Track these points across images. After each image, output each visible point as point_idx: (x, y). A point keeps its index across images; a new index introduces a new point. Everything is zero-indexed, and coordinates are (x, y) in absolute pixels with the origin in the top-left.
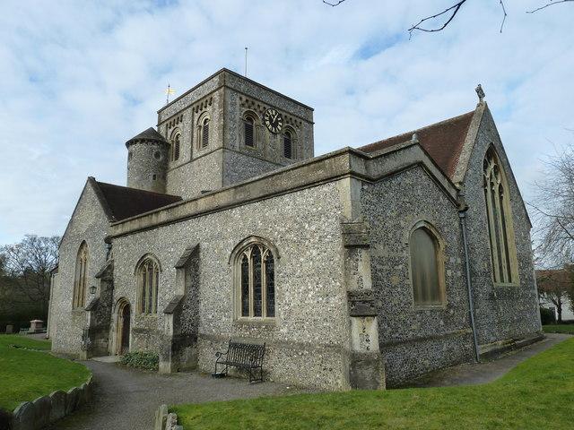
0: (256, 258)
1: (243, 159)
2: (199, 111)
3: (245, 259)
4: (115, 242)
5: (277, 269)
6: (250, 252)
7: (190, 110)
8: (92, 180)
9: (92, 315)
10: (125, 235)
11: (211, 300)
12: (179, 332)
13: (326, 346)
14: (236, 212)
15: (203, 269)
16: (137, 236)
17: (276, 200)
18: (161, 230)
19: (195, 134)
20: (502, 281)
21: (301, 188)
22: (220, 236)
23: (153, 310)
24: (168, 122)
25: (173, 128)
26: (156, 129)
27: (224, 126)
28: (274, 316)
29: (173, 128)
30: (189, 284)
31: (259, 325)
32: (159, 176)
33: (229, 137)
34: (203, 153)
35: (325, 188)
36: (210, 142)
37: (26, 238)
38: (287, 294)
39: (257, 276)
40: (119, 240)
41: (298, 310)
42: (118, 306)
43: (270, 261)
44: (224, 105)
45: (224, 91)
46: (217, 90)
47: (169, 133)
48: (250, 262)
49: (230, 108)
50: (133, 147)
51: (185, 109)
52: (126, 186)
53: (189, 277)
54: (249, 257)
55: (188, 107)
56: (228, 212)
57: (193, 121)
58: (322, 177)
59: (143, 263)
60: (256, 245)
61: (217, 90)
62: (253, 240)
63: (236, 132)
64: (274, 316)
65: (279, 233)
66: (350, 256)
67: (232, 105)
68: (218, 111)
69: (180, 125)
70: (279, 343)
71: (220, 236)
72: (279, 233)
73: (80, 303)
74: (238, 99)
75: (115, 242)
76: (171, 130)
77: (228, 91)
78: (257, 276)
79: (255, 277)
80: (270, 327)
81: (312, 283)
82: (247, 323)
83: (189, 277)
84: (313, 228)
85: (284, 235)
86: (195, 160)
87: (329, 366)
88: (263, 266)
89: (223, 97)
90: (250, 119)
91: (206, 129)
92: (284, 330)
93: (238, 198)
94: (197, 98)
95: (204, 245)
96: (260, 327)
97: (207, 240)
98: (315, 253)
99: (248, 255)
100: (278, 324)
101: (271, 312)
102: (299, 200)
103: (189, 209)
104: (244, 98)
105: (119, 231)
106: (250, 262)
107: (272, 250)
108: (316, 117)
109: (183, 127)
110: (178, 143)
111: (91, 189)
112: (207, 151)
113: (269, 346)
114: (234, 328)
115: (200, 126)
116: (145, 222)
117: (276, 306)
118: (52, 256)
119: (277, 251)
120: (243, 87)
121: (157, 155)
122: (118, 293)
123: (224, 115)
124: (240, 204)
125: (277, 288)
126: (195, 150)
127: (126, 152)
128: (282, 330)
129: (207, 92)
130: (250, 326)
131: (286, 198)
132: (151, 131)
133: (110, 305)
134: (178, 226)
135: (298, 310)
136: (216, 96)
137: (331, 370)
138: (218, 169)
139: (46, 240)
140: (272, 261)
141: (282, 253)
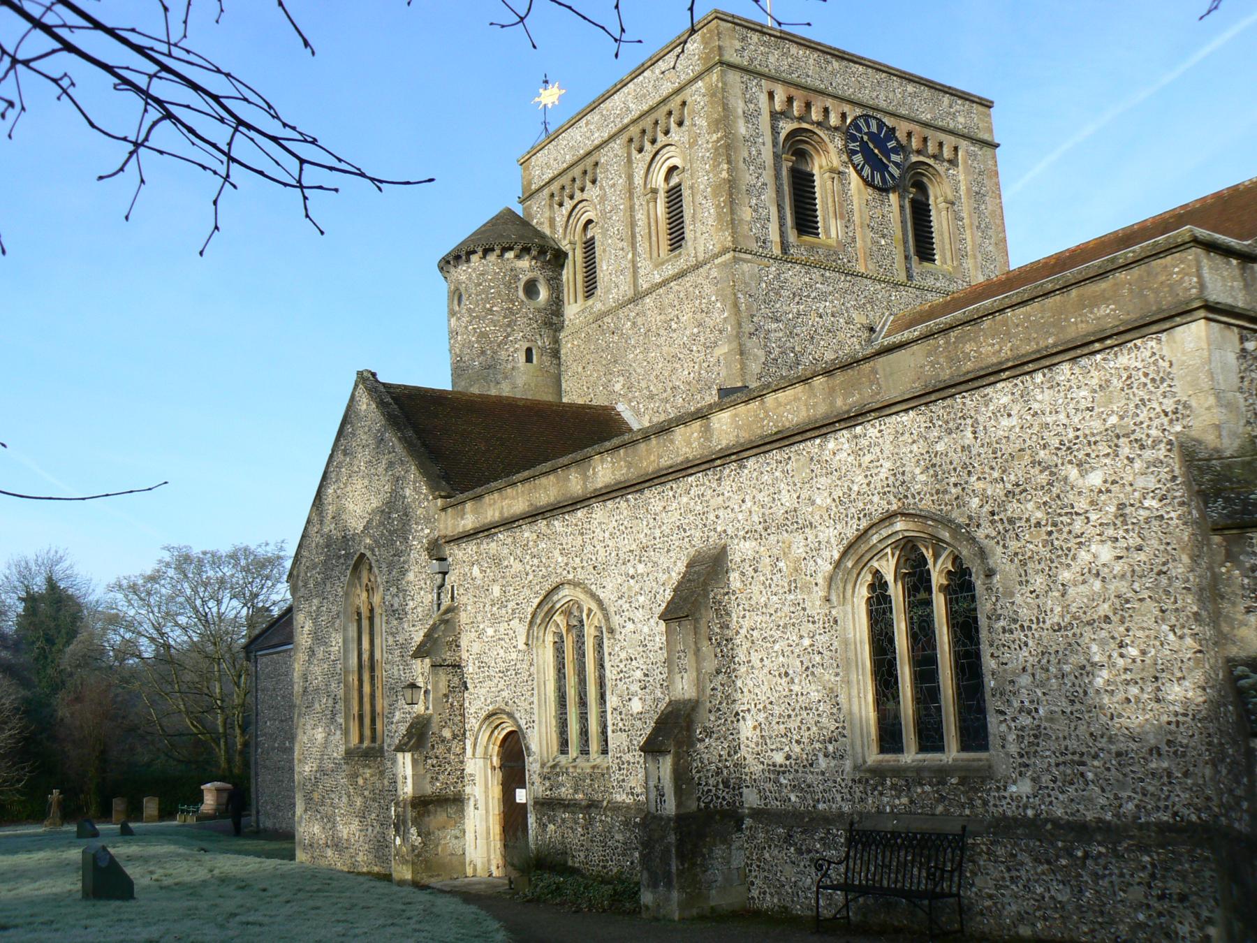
0: (917, 580)
1: (795, 277)
2: (648, 146)
3: (878, 585)
4: (457, 554)
5: (985, 606)
6: (893, 562)
7: (617, 146)
8: (367, 380)
9: (415, 762)
10: (484, 532)
11: (777, 710)
12: (683, 811)
13: (1162, 828)
14: (839, 446)
15: (742, 621)
16: (527, 533)
17: (968, 402)
18: (599, 513)
19: (640, 216)
20: (585, 752)
21: (1044, 360)
22: (794, 522)
23: (594, 746)
24: (555, 187)
25: (568, 204)
26: (519, 210)
27: (732, 185)
28: (985, 747)
29: (568, 204)
30: (710, 665)
31: (942, 773)
32: (542, 350)
33: (746, 214)
34: (670, 270)
35: (1128, 359)
36: (688, 235)
37: (167, 557)
38: (1025, 680)
39: (922, 633)
40: (471, 548)
41: (1061, 726)
42: (483, 737)
43: (960, 584)
44: (723, 121)
45: (723, 75)
46: (698, 77)
47: (560, 220)
48: (896, 592)
49: (742, 129)
50: (462, 273)
51: (605, 143)
52: (450, 389)
53: (706, 648)
54: (889, 578)
55: (612, 138)
56: (813, 447)
57: (630, 177)
58: (1110, 323)
59: (550, 614)
60: (908, 540)
61: (698, 77)
62: (900, 525)
63: (769, 196)
64: (985, 747)
65: (985, 499)
66: (1230, 557)
67: (748, 117)
68: (709, 140)
69: (592, 192)
70: (1005, 827)
71: (794, 522)
72: (985, 499)
73: (367, 732)
74: (763, 99)
75: (457, 554)
76: (565, 211)
77: (734, 77)
78: (922, 633)
79: (914, 637)
80: (974, 779)
81: (1102, 643)
82: (898, 772)
83: (706, 648)
84: (1095, 479)
85: (1002, 505)
86: (648, 292)
87: (1175, 887)
88: (939, 602)
89: (720, 97)
90: (801, 155)
91: (675, 196)
92: (1022, 788)
93: (839, 402)
94: (636, 109)
95: (742, 550)
96: (942, 782)
97: (749, 534)
98: (1105, 553)
99: (888, 567)
100: (1002, 769)
101: (974, 735)
102: (1043, 399)
103: (654, 456)
104: (780, 95)
105: (468, 520)
106: (896, 592)
107: (965, 552)
108: (1001, 125)
109: (603, 198)
110: (589, 246)
111: (365, 404)
112: (682, 263)
113: (975, 835)
114: (858, 789)
115: (655, 191)
116: (547, 490)
117: (992, 720)
118: (235, 603)
119: (982, 554)
120: (774, 60)
121: (531, 289)
122: (477, 703)
123: (727, 149)
124: (850, 419)
125: (989, 664)
126: (644, 265)
127: (441, 287)
128: (1014, 789)
129: (667, 88)
130: (915, 776)
131: (1001, 394)
132: (508, 216)
133: (460, 736)
134: (654, 499)
135: (1061, 726)
136: (697, 95)
137: (1183, 898)
138: (720, 315)
139: (216, 560)
140: (969, 587)
141: (998, 558)
